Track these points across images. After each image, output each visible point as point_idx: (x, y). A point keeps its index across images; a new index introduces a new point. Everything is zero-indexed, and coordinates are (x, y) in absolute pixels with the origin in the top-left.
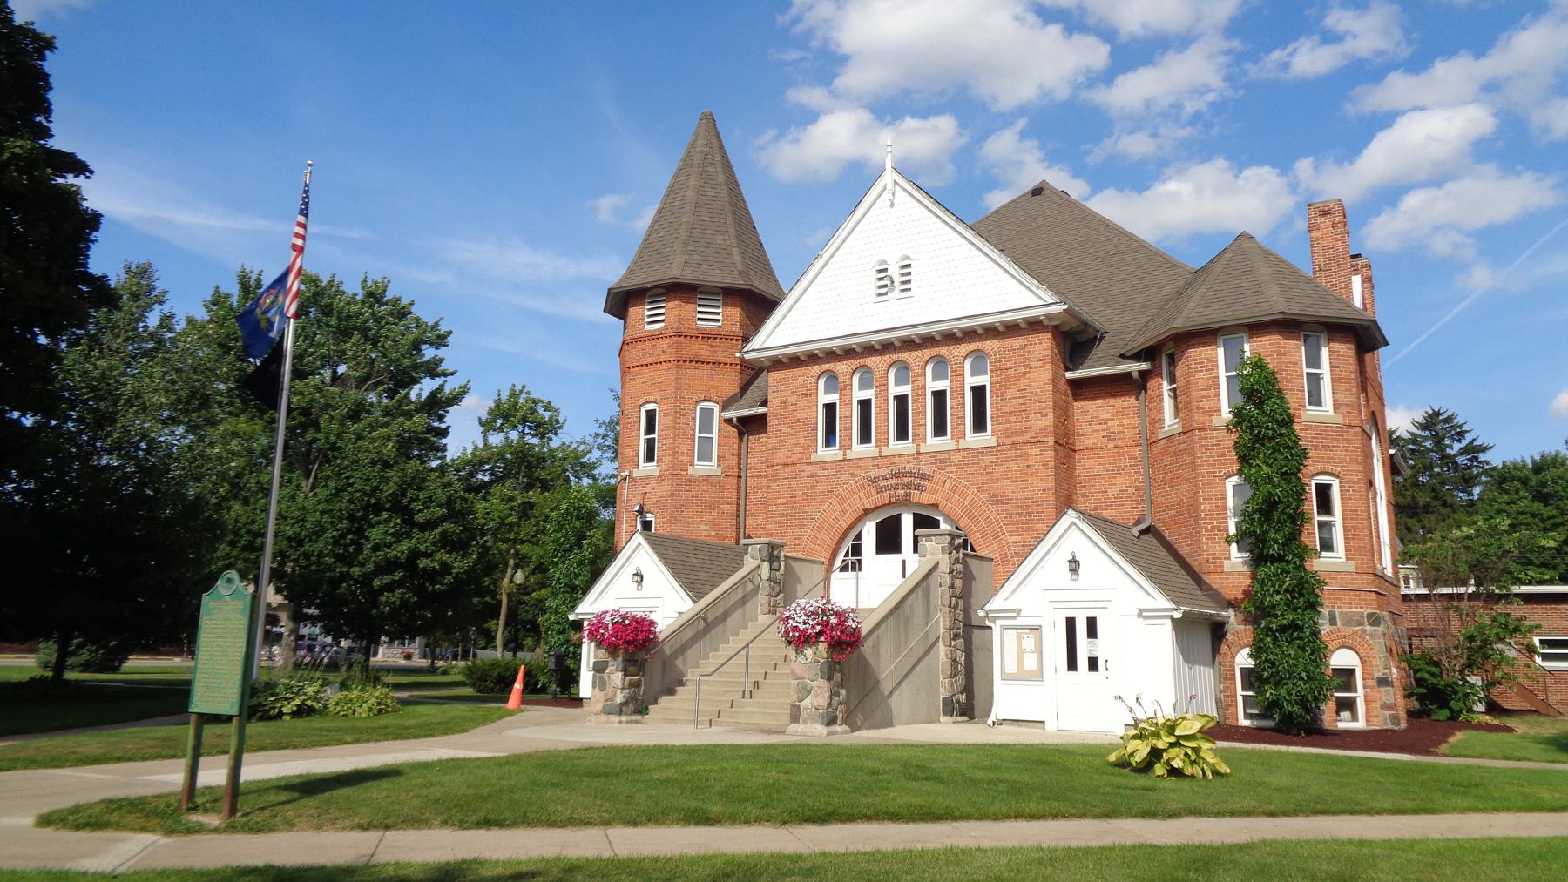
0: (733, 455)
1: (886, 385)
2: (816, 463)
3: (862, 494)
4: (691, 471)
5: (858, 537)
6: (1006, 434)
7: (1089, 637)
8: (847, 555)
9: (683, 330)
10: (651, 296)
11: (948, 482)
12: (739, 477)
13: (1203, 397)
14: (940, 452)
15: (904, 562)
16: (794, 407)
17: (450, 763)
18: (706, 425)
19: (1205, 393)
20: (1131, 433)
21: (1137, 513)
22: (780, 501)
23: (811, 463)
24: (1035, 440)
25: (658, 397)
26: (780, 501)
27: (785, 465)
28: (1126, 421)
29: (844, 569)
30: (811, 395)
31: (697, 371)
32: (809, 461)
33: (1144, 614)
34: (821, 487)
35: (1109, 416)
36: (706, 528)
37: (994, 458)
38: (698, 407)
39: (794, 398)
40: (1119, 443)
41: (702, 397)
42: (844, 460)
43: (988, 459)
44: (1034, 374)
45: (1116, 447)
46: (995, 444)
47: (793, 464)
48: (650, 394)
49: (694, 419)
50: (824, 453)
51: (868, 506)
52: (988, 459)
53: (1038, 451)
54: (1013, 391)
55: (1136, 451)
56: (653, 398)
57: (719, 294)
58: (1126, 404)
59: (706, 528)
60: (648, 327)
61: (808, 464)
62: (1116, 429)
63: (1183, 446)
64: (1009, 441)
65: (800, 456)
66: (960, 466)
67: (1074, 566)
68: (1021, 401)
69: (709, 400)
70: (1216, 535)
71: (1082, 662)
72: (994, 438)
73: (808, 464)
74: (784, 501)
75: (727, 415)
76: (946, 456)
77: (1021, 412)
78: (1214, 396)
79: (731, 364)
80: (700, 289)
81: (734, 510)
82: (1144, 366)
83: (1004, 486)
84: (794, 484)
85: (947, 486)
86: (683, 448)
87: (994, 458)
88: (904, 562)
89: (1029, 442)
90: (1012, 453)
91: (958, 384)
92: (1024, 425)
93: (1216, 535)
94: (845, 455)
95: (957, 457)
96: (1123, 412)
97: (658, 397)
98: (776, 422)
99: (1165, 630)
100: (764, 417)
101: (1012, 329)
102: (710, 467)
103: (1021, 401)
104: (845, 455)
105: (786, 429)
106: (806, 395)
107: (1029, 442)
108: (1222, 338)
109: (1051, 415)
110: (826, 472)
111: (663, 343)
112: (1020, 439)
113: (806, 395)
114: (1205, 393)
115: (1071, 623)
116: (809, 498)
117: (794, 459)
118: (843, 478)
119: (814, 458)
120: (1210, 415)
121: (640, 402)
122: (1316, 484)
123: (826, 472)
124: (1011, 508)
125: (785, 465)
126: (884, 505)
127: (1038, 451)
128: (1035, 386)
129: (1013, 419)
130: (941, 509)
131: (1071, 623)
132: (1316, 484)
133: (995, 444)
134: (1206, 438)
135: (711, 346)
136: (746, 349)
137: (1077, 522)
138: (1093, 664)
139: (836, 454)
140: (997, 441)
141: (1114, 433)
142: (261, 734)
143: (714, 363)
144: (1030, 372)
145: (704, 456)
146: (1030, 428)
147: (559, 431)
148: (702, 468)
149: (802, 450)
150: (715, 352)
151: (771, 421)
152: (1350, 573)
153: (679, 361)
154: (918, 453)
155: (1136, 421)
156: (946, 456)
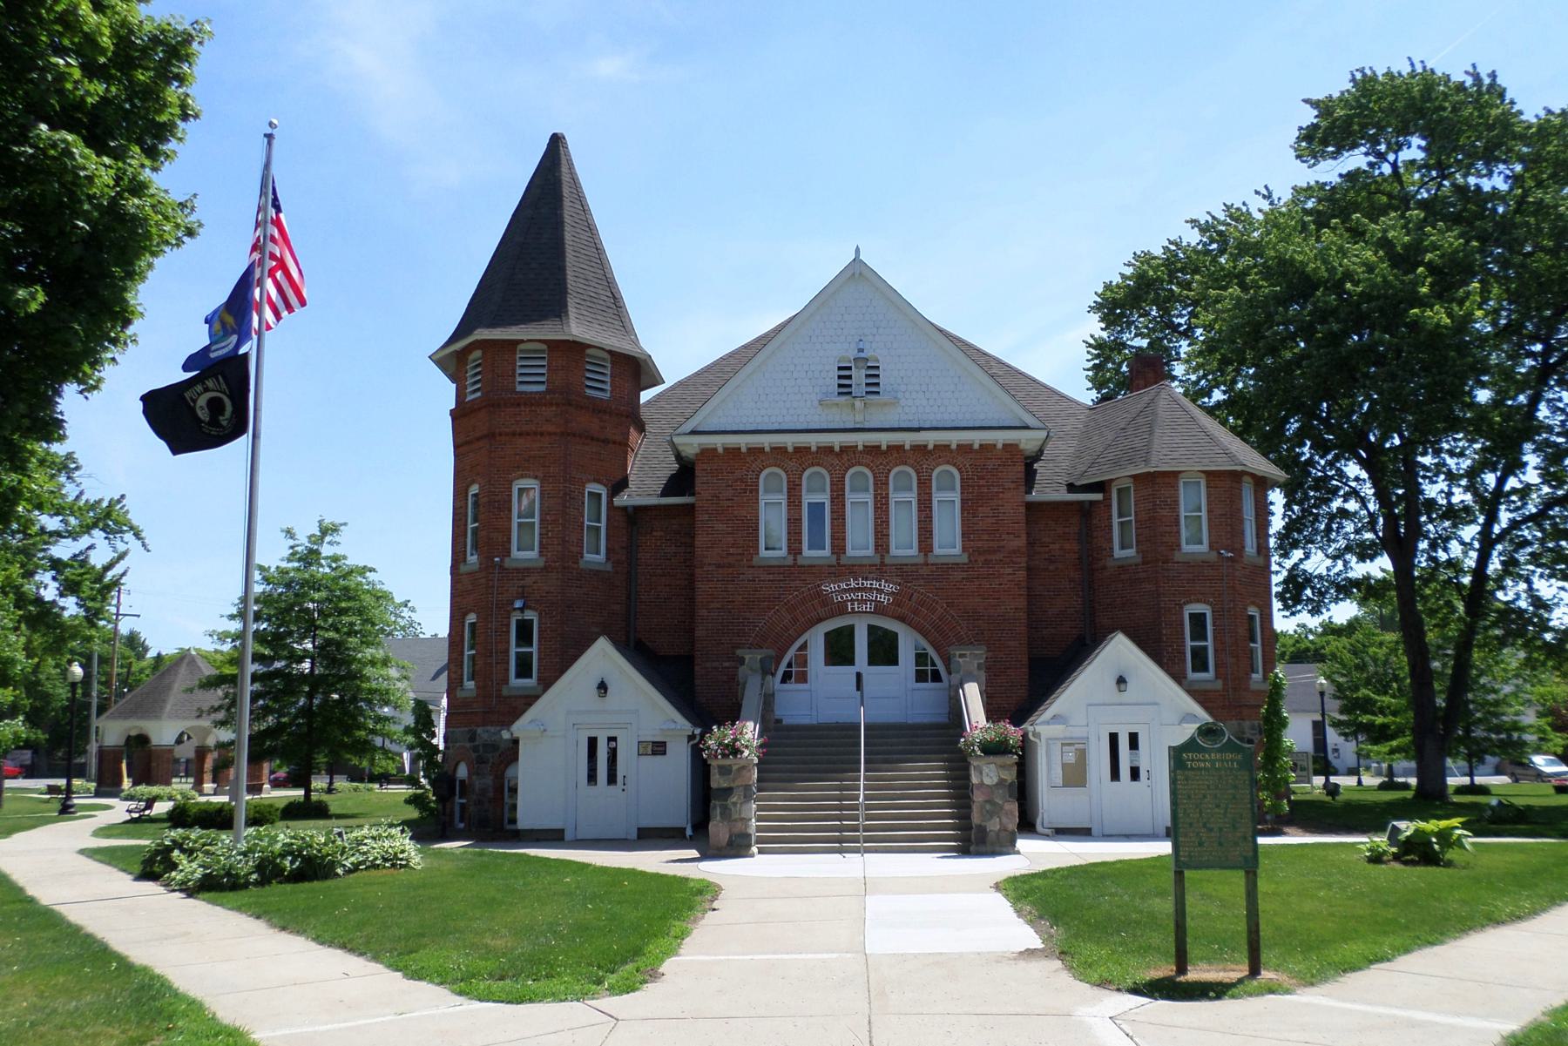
5: (804, 647)
7: (1131, 749)
8: (790, 665)
14: (907, 565)
15: (859, 675)
16: (729, 503)
17: (327, 936)
19: (1168, 529)
22: (712, 605)
26: (712, 605)
28: (1067, 546)
37: (964, 575)
42: (795, 565)
45: (1057, 569)
46: (966, 561)
52: (958, 575)
53: (1009, 570)
58: (1067, 530)
60: (520, 388)
63: (1143, 575)
65: (739, 557)
71: (1125, 771)
74: (718, 605)
76: (914, 568)
80: (589, 351)
87: (964, 575)
88: (859, 675)
94: (795, 560)
98: (706, 517)
104: (795, 560)
105: (721, 527)
109: (1024, 537)
110: (771, 577)
114: (1168, 529)
115: (1114, 738)
122: (1190, 614)
123: (771, 577)
129: (986, 537)
131: (1114, 738)
132: (1190, 614)
134: (1168, 570)
138: (1135, 774)
140: (969, 557)
142: (1208, 971)
143: (603, 441)
146: (1003, 547)
147: (77, 473)
149: (740, 551)
151: (701, 517)
154: (882, 563)
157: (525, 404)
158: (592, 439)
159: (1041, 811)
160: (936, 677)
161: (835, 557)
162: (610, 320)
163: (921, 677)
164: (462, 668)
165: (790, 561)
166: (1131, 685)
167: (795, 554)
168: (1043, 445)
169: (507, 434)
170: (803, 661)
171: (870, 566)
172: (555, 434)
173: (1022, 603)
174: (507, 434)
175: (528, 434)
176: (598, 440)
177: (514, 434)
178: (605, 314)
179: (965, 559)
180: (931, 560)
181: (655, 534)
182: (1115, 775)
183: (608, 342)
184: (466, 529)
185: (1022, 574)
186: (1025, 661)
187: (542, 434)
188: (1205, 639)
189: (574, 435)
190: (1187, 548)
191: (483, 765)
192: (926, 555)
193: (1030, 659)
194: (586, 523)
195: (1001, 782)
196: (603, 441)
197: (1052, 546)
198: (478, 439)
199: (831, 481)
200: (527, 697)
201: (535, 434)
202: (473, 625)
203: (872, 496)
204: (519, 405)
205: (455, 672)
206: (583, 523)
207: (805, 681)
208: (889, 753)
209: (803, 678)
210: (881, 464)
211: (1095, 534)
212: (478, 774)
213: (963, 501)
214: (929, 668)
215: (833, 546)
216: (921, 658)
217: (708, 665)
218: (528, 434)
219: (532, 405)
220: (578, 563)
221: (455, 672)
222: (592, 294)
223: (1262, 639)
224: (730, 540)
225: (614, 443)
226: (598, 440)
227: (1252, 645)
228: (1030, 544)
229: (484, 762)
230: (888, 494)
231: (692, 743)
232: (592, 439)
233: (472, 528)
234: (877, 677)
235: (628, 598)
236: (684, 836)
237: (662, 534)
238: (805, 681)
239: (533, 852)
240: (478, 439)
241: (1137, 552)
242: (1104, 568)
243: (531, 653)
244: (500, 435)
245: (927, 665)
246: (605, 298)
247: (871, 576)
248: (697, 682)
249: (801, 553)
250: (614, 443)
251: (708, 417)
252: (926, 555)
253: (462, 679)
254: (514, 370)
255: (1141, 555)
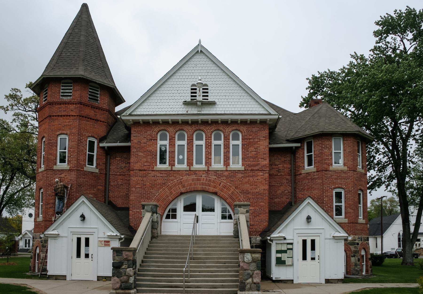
0: (103, 164)
1: (193, 139)
2: (157, 171)
3: (180, 186)
4: (85, 169)
6: (249, 166)
8: (169, 212)
9: (83, 102)
10: (63, 83)
11: (222, 184)
12: (106, 174)
13: (326, 159)
14: (218, 171)
16: (145, 145)
18: (91, 149)
20: (287, 170)
21: (288, 200)
22: (137, 186)
23: (154, 171)
24: (261, 169)
25: (68, 132)
26: (137, 186)
27: (140, 170)
28: (285, 166)
29: (168, 217)
30: (154, 140)
31: (88, 123)
32: (153, 169)
33: (335, 238)
34: (159, 181)
35: (279, 163)
36: (92, 196)
38: (88, 140)
39: (145, 140)
40: (283, 174)
41: (90, 135)
42: (171, 170)
43: (240, 175)
44: (261, 143)
45: (281, 175)
46: (243, 169)
47: (145, 170)
48: (63, 130)
49: (86, 144)
50: (160, 166)
51: (183, 191)
52: (240, 175)
53: (262, 174)
54: (252, 149)
55: (289, 177)
56: (65, 132)
57: (98, 88)
58: (286, 159)
59: (92, 196)
61: (152, 171)
62: (281, 168)
63: (316, 177)
64: (250, 169)
65: (148, 167)
66: (227, 177)
67: (83, 217)
68: (255, 153)
69: (93, 137)
70: (329, 209)
72: (243, 167)
73: (152, 171)
74: (140, 186)
75: (101, 145)
77: (255, 157)
78: (330, 159)
79: (103, 122)
81: (103, 189)
82: (299, 145)
83: (247, 187)
84: (145, 179)
85: (221, 185)
86: (82, 158)
89: (258, 170)
90: (251, 174)
91: (227, 143)
92: (256, 163)
93: (329, 209)
95: (226, 173)
96: (284, 162)
97: (68, 132)
98: (135, 150)
99: (341, 246)
100: (128, 149)
101: (253, 122)
102: (93, 168)
103: (255, 153)
106: (151, 140)
107: (258, 170)
108: (333, 138)
109: (268, 160)
110: (162, 175)
111: (72, 107)
112: (255, 168)
113: (151, 140)
116: (153, 186)
117: (145, 168)
118: (170, 178)
119: (155, 168)
120: (329, 166)
121: (58, 133)
123: (162, 175)
124: (250, 196)
125: (140, 170)
126: (194, 191)
127: (262, 174)
128: (261, 147)
129: (252, 160)
130: (218, 194)
133: (243, 169)
135: (95, 112)
136: (123, 114)
137: (310, 202)
139: (167, 168)
140: (245, 168)
141: (280, 170)
143: (96, 120)
144: (260, 142)
145: (91, 162)
146: (259, 164)
148: (89, 168)
149: (149, 164)
150: (96, 115)
151: (133, 150)
152: (346, 223)
153: (80, 116)
155: (289, 166)
156: (221, 172)
157: (63, 104)
158: (91, 119)
159: (272, 272)
160: (230, 217)
161: (170, 167)
162: (101, 73)
163: (224, 217)
164: (39, 210)
165: (169, 168)
166: (79, 219)
167: (172, 166)
168: (276, 123)
169: (56, 116)
170: (174, 210)
171: (203, 171)
172: (75, 116)
173: (267, 187)
174: (56, 116)
175: (64, 116)
176: (93, 119)
177: (58, 116)
178: (98, 70)
179: (243, 168)
180: (229, 169)
181: (117, 158)
182: (79, 255)
183: (101, 80)
184: (41, 155)
185: (267, 175)
186: (267, 211)
187: (70, 116)
188: (341, 202)
189: (83, 117)
190: (335, 166)
191: (44, 248)
192: (227, 167)
193: (269, 211)
194: (88, 153)
195: (254, 261)
196: (96, 120)
197: (279, 166)
198: (45, 119)
199: (187, 136)
200: (340, 226)
201: (67, 116)
202: (42, 192)
203: (205, 143)
204: (61, 104)
205: (37, 212)
206: (86, 152)
207: (175, 218)
208: (205, 247)
209: (174, 217)
210: (208, 129)
211: (297, 161)
212: (42, 251)
213: (243, 145)
214: (227, 214)
215: (206, 163)
216: (224, 210)
217: (135, 210)
218: (64, 116)
219: (66, 104)
220: (83, 169)
221: (37, 212)
222: (93, 62)
223: (363, 203)
224: (145, 160)
225: (101, 121)
226: (93, 119)
227: (359, 205)
228: (271, 165)
229: (44, 247)
230: (211, 142)
231: (121, 241)
232: (91, 119)
233: (312, 152)
234: (204, 217)
235: (106, 184)
236: (38, 277)
237: (120, 159)
238: (175, 218)
239: (143, 288)
240: (45, 119)
241: (314, 167)
242: (301, 174)
243: (342, 205)
244: (53, 116)
245: (226, 213)
246: (99, 64)
247: (203, 175)
248: (130, 217)
249: (174, 166)
250: (101, 121)
251: (139, 112)
252: (227, 167)
253: (39, 214)
254: (59, 91)
255: (316, 168)
